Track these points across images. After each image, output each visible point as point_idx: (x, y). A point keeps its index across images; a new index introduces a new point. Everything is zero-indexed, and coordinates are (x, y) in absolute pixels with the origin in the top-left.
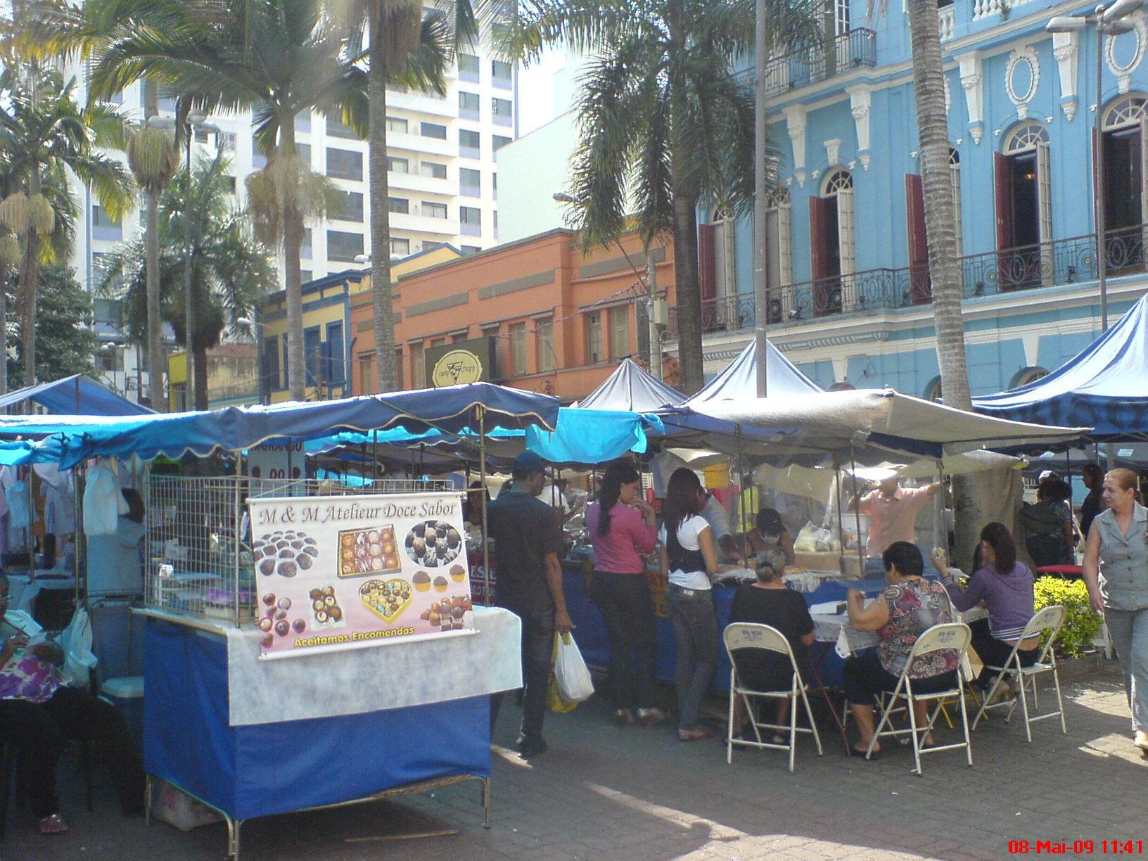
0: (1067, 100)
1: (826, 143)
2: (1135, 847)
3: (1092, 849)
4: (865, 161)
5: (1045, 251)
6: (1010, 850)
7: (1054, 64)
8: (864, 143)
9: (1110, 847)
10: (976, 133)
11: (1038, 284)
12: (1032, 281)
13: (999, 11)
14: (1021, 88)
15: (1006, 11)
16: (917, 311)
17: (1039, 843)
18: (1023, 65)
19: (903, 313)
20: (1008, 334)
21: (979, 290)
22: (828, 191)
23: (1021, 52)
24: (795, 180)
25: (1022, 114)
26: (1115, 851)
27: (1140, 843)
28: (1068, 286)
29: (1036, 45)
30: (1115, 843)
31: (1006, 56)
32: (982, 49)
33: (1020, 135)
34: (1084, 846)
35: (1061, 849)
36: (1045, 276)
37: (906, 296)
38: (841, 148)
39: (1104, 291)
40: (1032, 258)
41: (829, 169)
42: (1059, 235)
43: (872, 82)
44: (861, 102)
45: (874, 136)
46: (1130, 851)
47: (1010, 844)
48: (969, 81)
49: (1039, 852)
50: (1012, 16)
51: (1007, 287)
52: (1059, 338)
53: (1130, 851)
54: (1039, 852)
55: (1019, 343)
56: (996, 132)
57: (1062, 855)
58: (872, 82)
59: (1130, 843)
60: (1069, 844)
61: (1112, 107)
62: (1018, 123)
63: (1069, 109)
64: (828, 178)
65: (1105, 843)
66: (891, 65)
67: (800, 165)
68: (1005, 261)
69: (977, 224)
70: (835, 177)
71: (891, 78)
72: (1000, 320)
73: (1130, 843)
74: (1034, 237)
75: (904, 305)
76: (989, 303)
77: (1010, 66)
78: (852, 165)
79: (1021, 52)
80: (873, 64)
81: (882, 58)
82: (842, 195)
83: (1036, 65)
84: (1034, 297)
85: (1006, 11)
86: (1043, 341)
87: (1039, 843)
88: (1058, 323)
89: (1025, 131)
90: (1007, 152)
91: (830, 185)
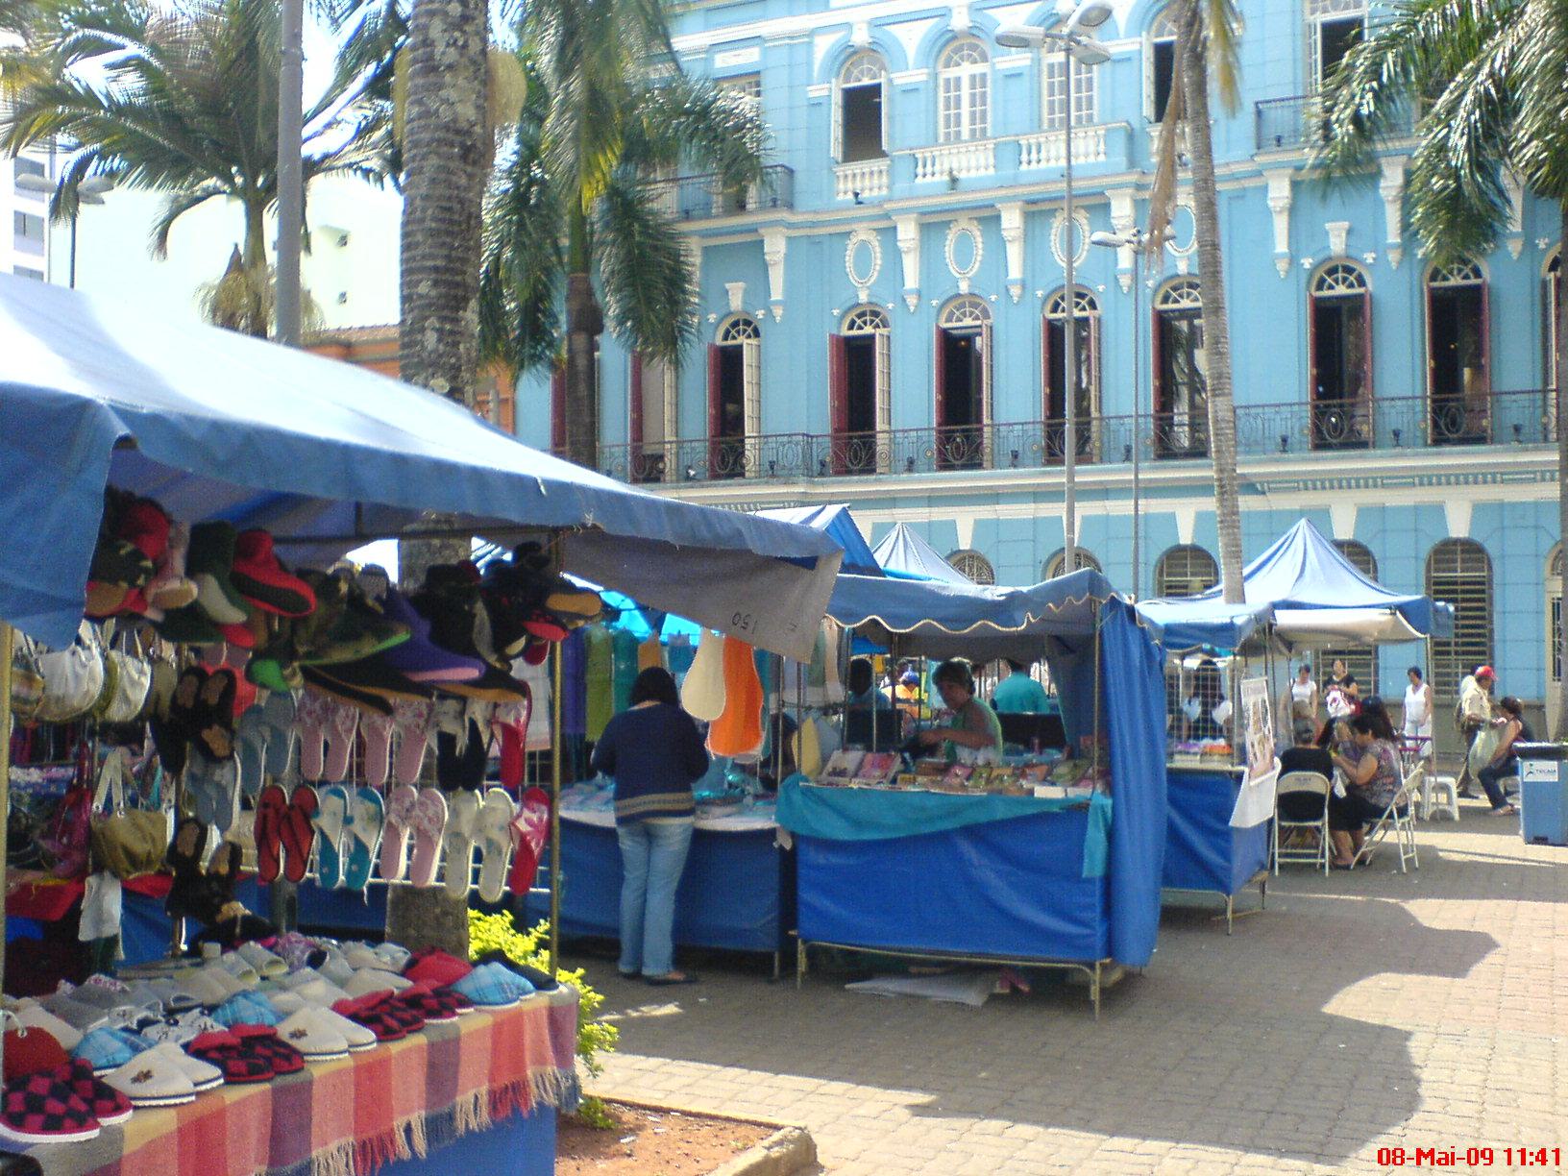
0: (1014, 282)
1: (728, 286)
2: (1550, 1156)
3: (1491, 1159)
4: (778, 312)
5: (881, 440)
6: (1380, 1161)
7: (1002, 243)
8: (777, 293)
9: (1516, 1157)
10: (912, 301)
11: (979, 466)
12: (1354, 442)
13: (946, 178)
14: (963, 260)
15: (954, 181)
16: (1343, 458)
17: (1419, 1152)
18: (964, 239)
19: (822, 484)
20: (940, 514)
21: (911, 466)
22: (726, 338)
23: (964, 224)
24: (769, 313)
25: (964, 287)
26: (1523, 1163)
27: (1557, 1151)
28: (1012, 470)
29: (980, 220)
30: (1523, 1151)
31: (947, 224)
32: (924, 214)
33: (859, 316)
34: (1479, 1156)
35: (1449, 1159)
36: (881, 463)
37: (823, 464)
38: (746, 292)
39: (1071, 479)
40: (869, 444)
41: (730, 313)
42: (769, 428)
43: (790, 226)
44: (775, 247)
45: (789, 286)
46: (1544, 1162)
47: (1380, 1153)
48: (1123, 222)
49: (1419, 1163)
50: (960, 186)
51: (945, 465)
52: (997, 522)
53: (1544, 1162)
54: (1419, 1163)
55: (952, 525)
56: (934, 303)
57: (1449, 1168)
58: (790, 226)
59: (1543, 1152)
60: (1411, 1152)
61: (950, 307)
62: (959, 295)
63: (1015, 291)
64: (726, 325)
65: (1509, 1151)
66: (815, 212)
67: (716, 301)
68: (945, 438)
69: (908, 395)
70: (735, 324)
71: (814, 225)
72: (933, 499)
73: (1543, 1152)
74: (871, 425)
75: (822, 474)
76: (920, 481)
77: (951, 236)
78: (760, 314)
79: (964, 224)
80: (790, 206)
81: (801, 201)
82: (748, 345)
83: (979, 239)
84: (972, 479)
85: (954, 181)
86: (979, 524)
87: (1419, 1152)
88: (1107, 503)
89: (963, 305)
90: (845, 332)
91: (727, 332)
